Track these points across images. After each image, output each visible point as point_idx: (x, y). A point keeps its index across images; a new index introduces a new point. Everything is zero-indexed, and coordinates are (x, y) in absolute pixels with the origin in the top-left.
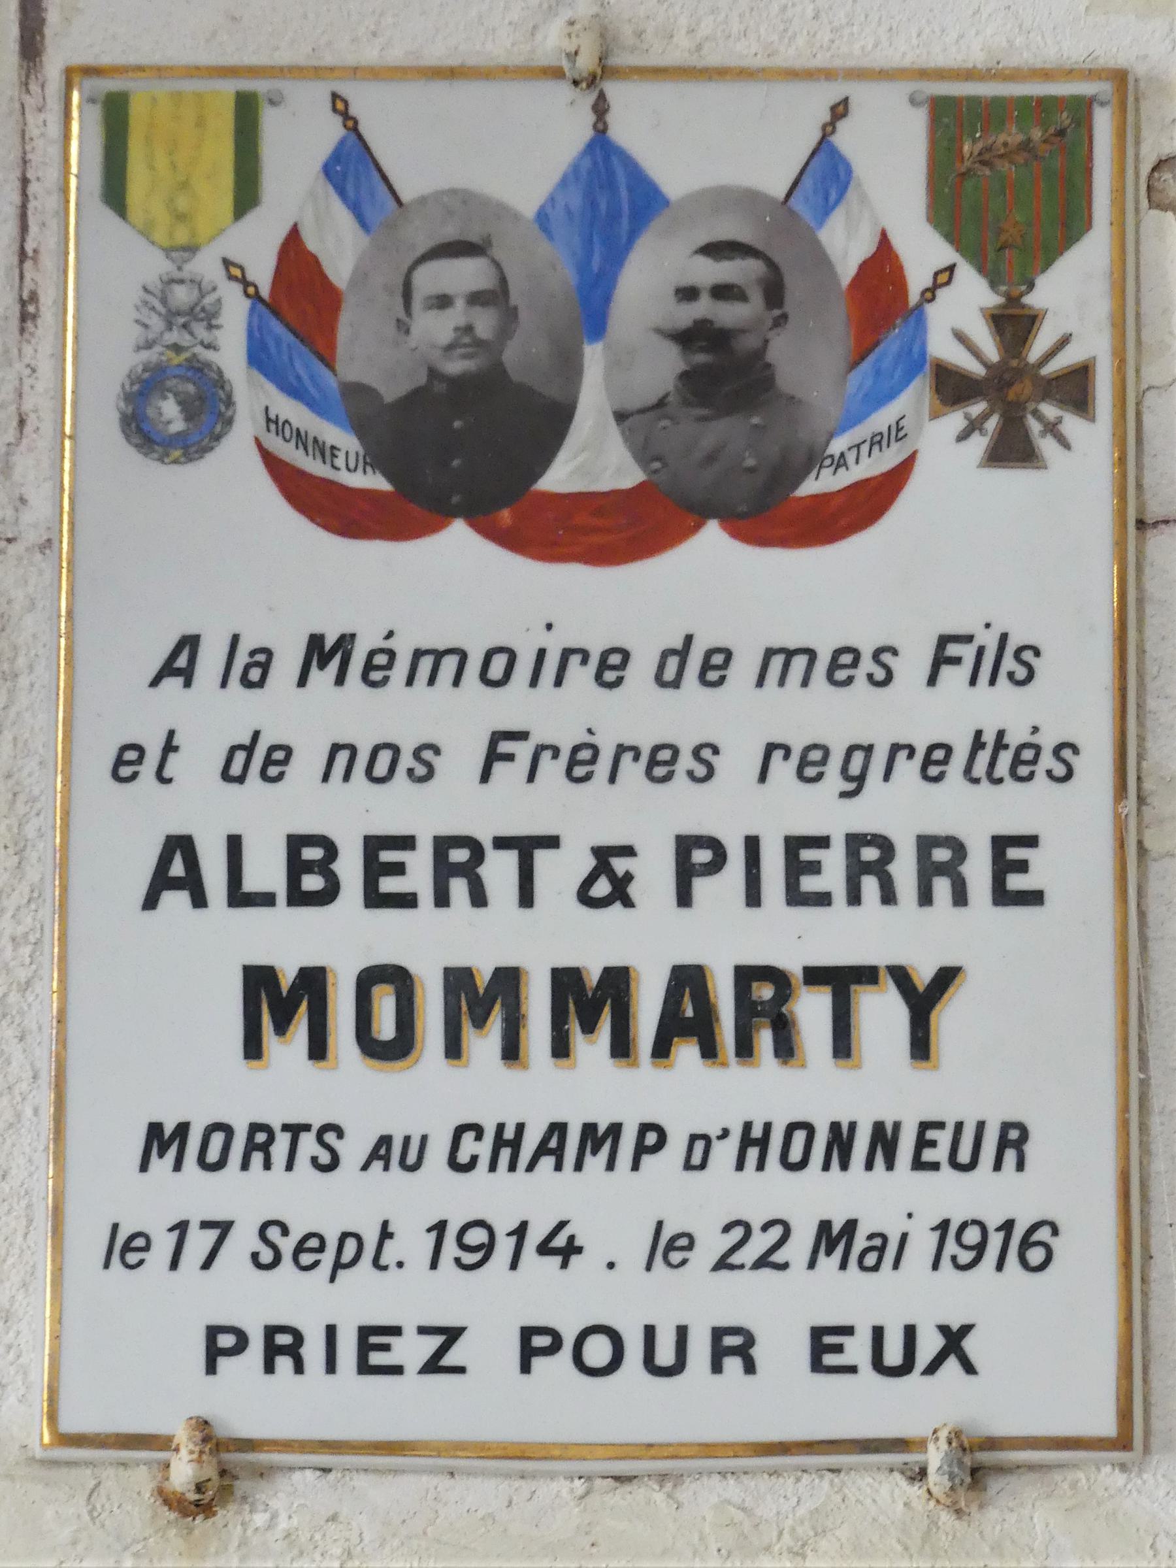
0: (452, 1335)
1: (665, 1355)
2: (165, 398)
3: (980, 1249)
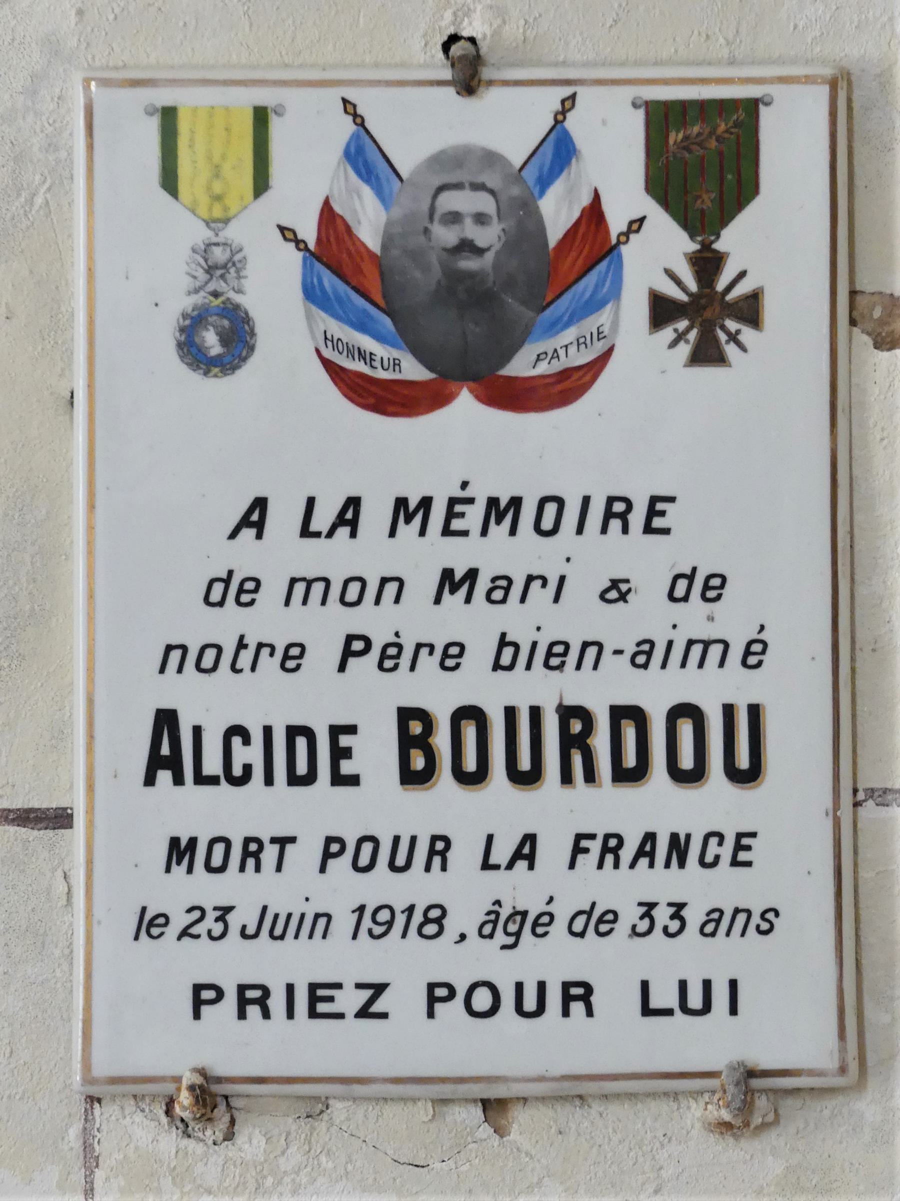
0: (379, 989)
1: (530, 1004)
2: (208, 330)
3: (390, 924)
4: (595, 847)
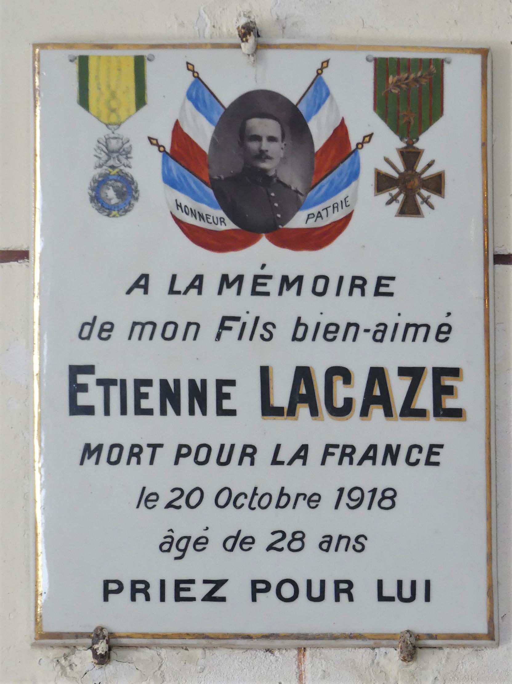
0: (219, 583)
1: (316, 593)
2: (109, 189)
4: (338, 452)
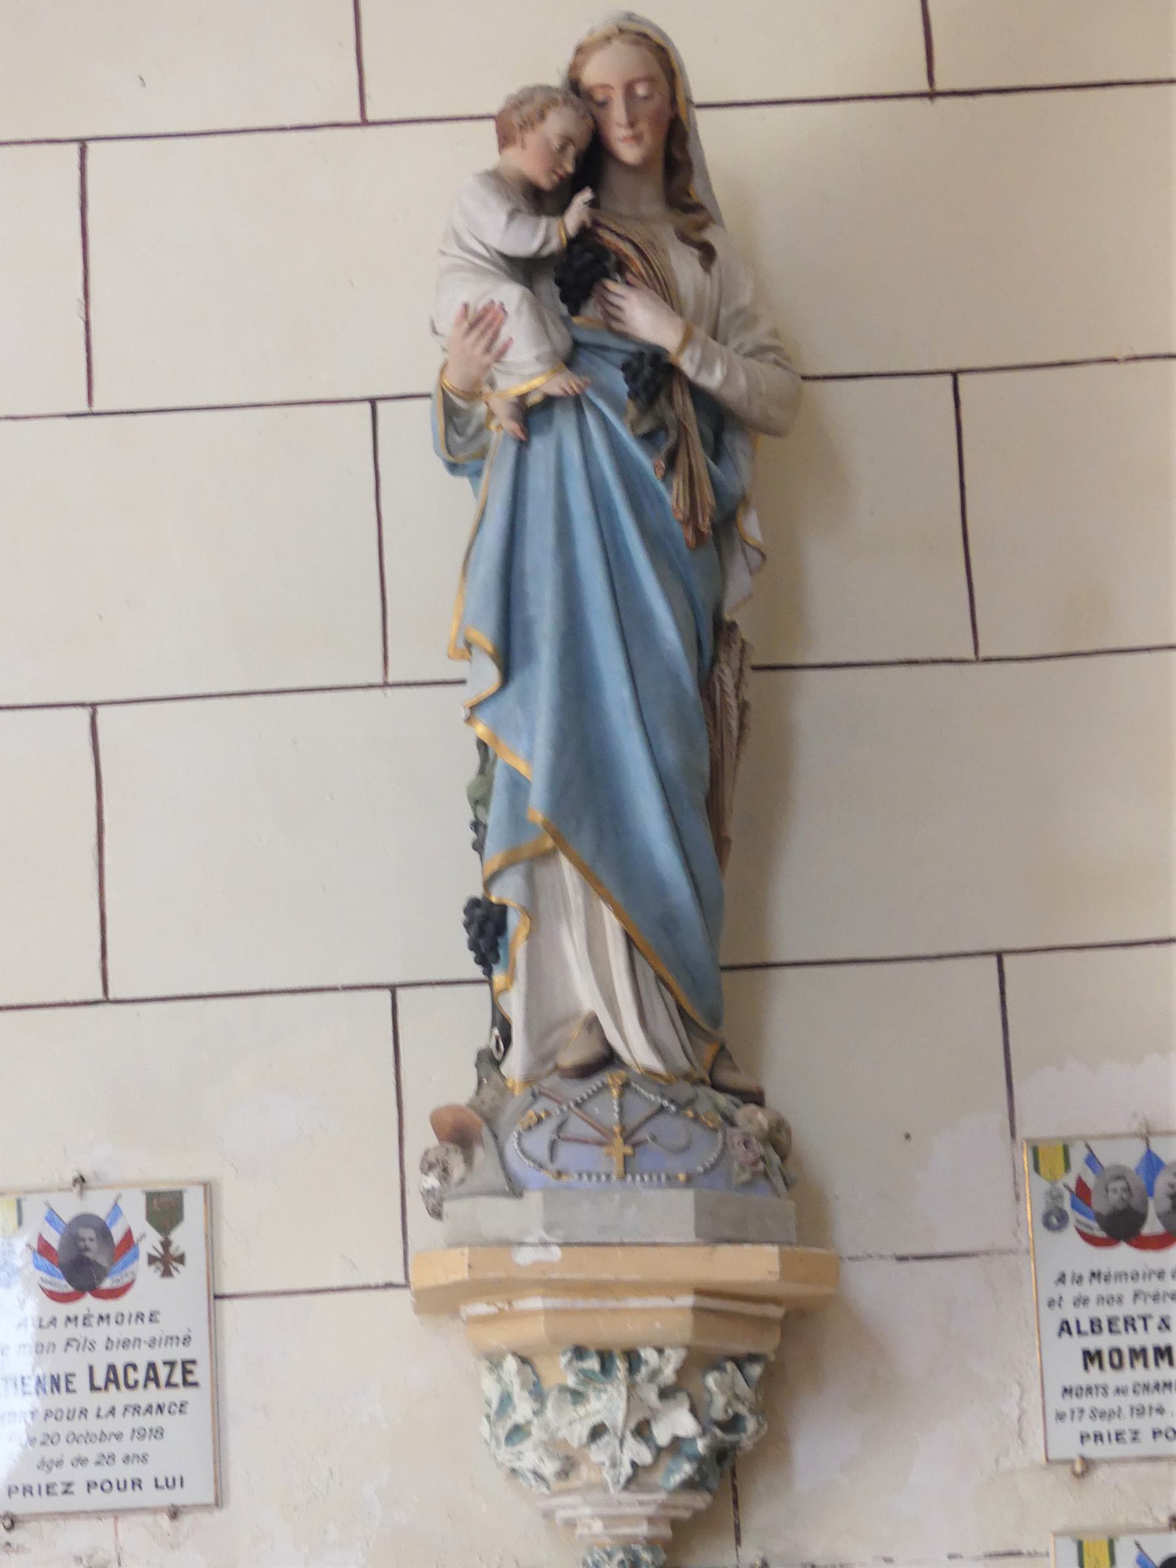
1: (122, 1485)
